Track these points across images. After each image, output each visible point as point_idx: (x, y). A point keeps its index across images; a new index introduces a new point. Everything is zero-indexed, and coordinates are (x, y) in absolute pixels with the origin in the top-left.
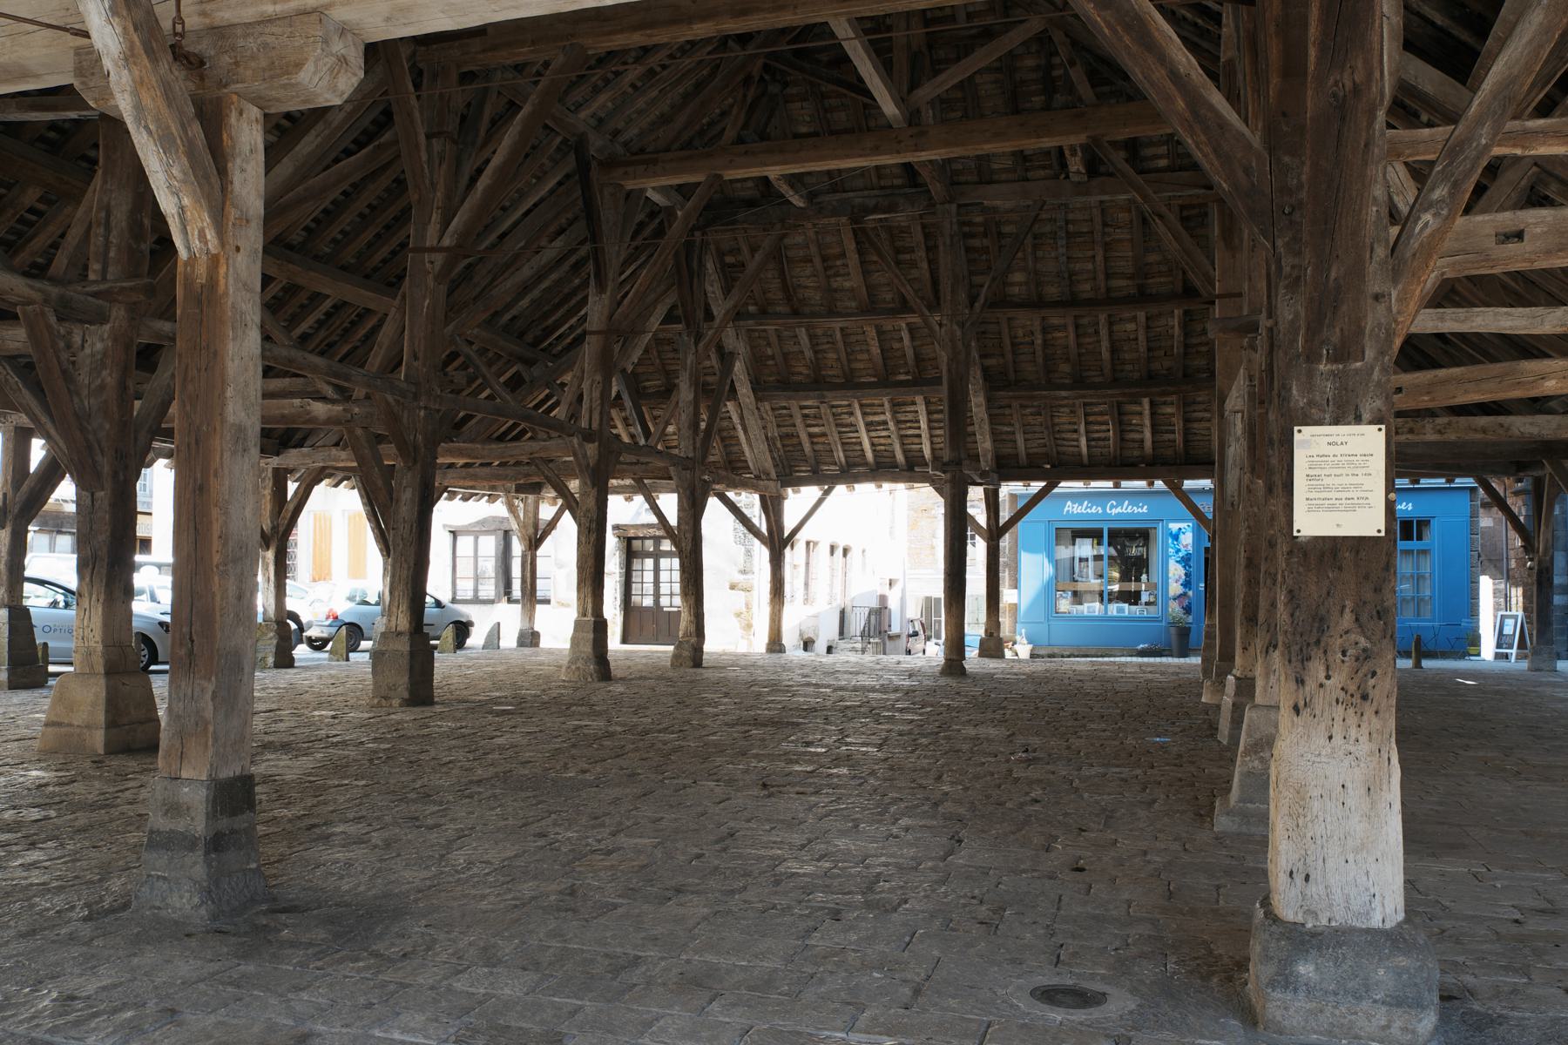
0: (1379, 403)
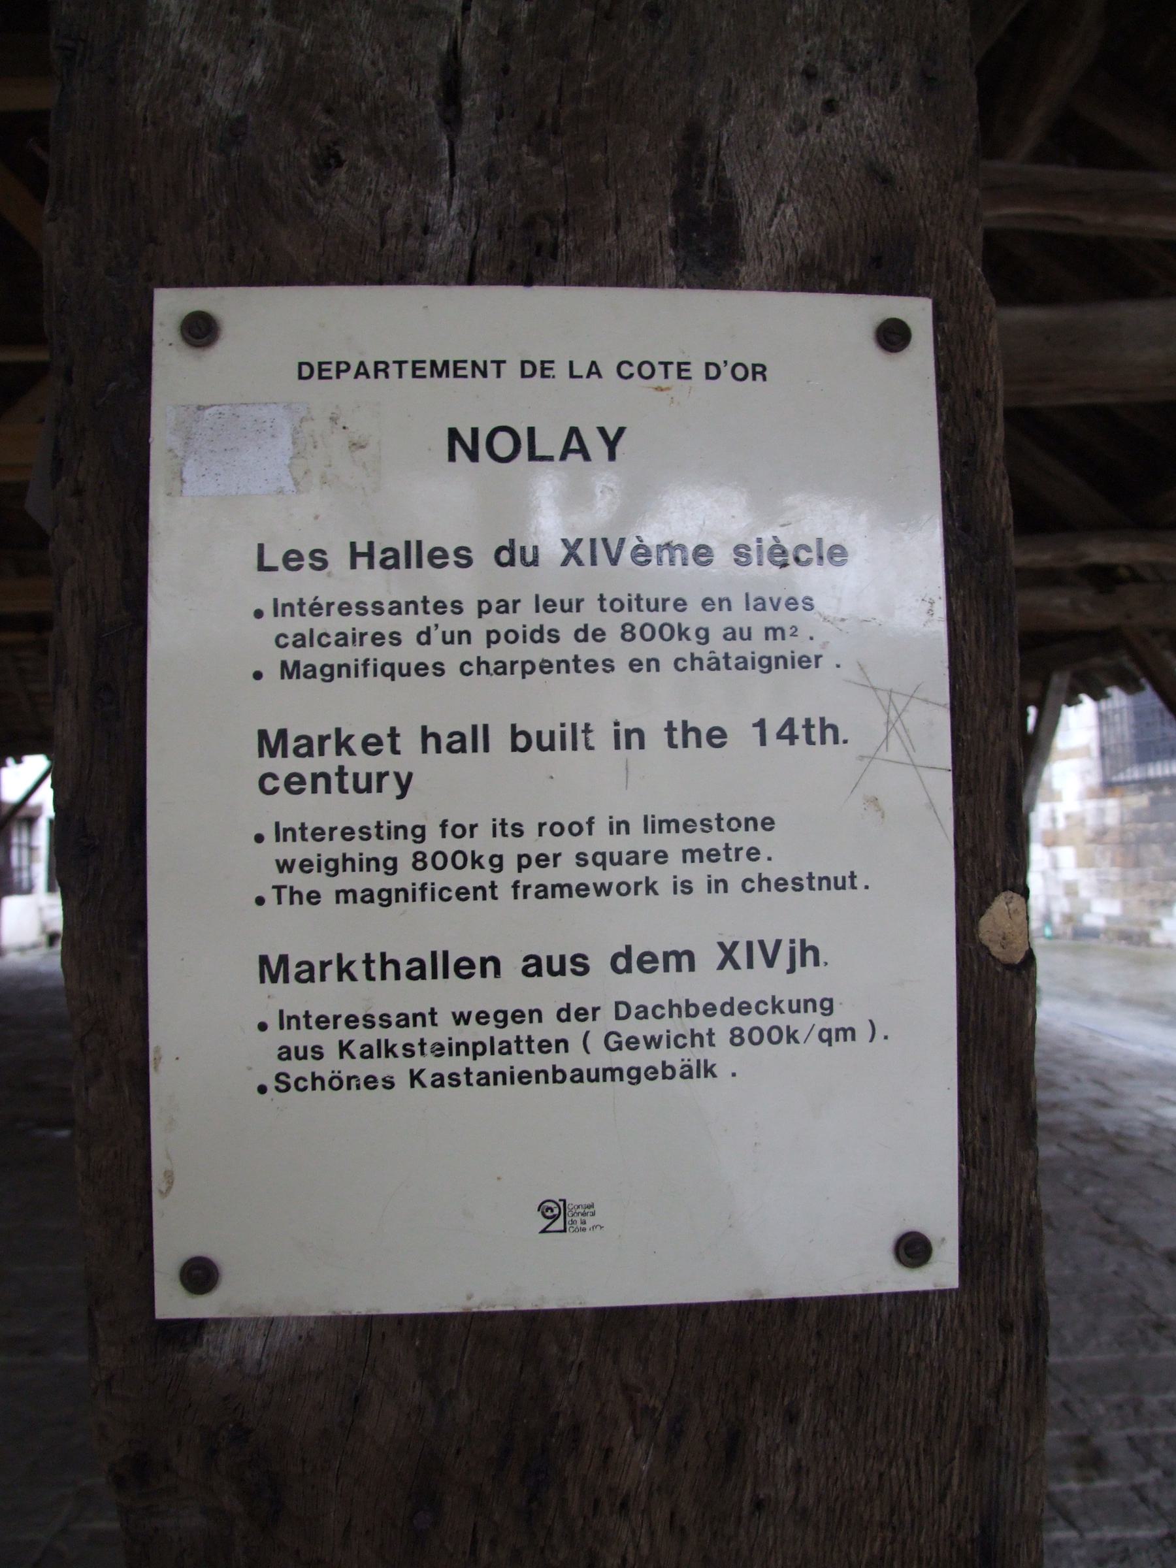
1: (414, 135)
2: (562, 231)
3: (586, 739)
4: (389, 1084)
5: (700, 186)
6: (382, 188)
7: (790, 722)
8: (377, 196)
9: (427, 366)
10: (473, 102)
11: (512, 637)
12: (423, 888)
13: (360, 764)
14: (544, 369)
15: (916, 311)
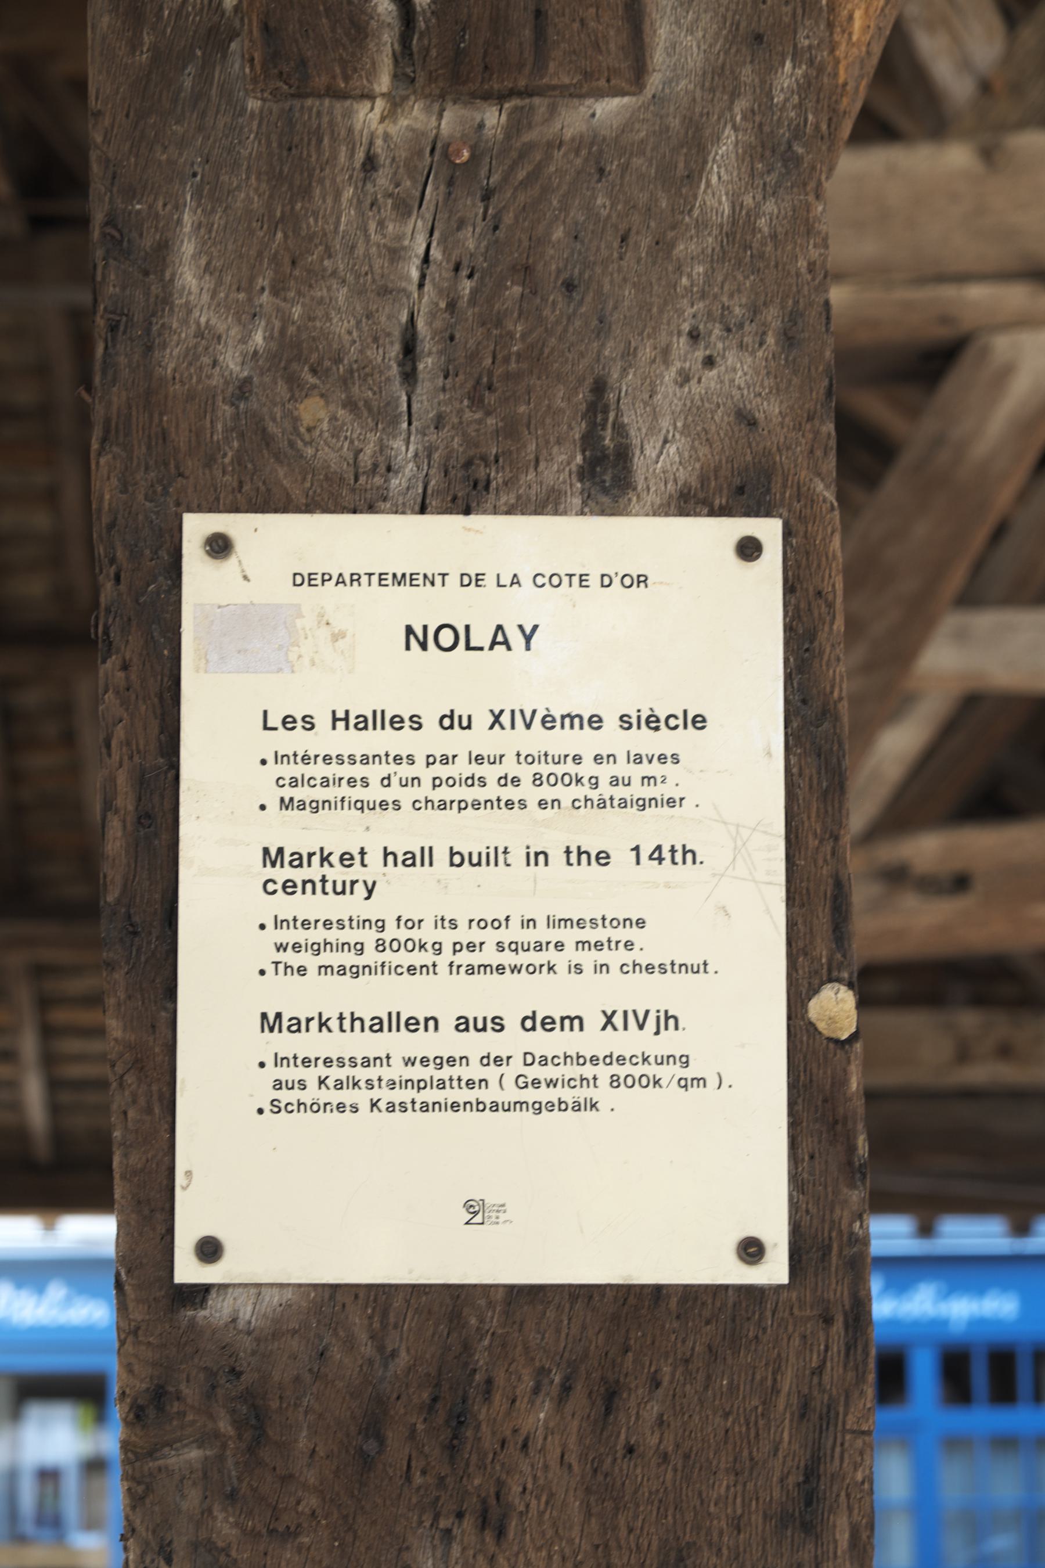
0: (739, 372)
1: (381, 392)
2: (494, 469)
3: (505, 859)
4: (355, 1109)
5: (604, 429)
6: (355, 436)
7: (659, 848)
8: (352, 442)
9: (390, 577)
10: (426, 364)
11: (451, 782)
12: (383, 965)
13: (337, 873)
14: (478, 579)
15: (769, 531)
